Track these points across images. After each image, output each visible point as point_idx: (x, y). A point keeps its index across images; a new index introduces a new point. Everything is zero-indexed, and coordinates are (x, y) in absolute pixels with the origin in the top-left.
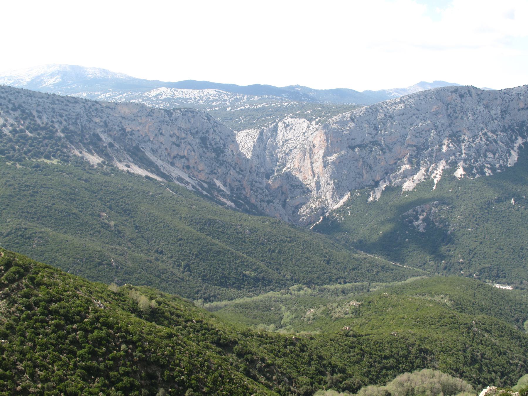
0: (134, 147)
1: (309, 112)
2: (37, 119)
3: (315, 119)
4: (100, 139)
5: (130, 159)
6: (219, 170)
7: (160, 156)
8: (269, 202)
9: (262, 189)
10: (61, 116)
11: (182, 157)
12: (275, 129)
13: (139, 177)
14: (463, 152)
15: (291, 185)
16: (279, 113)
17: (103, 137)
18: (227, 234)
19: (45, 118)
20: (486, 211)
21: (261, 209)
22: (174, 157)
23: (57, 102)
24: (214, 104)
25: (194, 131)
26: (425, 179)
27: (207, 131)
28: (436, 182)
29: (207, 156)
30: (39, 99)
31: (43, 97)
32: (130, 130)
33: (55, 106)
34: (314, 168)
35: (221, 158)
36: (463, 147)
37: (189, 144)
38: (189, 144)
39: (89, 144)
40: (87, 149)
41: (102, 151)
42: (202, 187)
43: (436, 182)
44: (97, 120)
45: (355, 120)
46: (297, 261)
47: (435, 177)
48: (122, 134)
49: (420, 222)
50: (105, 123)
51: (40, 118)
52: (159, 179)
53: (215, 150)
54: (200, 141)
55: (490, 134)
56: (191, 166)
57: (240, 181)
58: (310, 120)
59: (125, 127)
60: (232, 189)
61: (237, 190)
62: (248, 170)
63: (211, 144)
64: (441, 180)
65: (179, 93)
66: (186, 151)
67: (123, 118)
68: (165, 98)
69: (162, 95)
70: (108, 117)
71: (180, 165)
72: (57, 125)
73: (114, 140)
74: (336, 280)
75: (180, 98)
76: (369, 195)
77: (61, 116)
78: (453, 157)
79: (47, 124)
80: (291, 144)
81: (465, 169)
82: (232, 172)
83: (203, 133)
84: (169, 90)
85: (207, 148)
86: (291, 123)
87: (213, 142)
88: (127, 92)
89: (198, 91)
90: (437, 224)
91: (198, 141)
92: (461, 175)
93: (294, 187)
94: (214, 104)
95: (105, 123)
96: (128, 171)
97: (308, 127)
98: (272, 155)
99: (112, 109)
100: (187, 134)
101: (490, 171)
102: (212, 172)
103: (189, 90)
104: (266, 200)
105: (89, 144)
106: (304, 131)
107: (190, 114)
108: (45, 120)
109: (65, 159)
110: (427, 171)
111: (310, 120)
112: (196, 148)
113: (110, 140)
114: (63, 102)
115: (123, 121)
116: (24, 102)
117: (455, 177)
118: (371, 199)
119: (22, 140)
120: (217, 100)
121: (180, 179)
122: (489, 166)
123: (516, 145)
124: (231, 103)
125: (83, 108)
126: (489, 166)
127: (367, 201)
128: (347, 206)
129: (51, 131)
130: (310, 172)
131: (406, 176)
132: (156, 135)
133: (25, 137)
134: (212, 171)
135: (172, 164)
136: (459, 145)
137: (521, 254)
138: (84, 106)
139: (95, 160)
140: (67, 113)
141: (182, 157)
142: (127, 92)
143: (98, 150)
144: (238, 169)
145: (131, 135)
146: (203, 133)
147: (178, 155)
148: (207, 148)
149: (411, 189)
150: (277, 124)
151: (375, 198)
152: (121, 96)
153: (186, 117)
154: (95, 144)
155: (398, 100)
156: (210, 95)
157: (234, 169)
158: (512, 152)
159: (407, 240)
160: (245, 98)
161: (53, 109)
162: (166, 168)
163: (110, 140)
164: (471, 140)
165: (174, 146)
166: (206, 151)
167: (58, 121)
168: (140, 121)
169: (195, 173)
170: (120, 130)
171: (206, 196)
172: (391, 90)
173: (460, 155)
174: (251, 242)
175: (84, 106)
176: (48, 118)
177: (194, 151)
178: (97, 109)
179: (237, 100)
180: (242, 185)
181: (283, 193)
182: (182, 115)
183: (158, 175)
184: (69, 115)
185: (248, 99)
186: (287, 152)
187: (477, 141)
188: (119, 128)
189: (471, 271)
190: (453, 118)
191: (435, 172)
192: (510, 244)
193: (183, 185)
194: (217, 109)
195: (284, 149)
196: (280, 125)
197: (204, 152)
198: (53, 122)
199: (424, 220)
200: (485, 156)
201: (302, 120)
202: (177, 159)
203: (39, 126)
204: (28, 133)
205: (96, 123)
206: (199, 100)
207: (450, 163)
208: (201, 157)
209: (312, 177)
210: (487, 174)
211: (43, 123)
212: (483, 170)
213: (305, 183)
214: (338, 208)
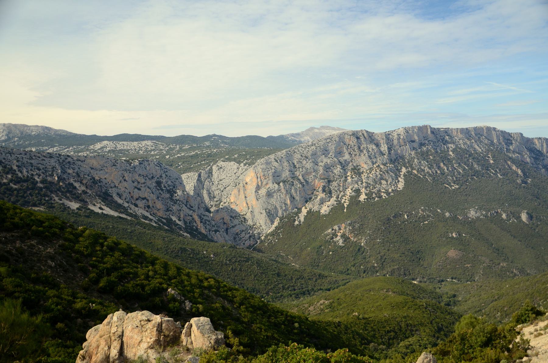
0: (104, 193)
1: (236, 156)
2: (17, 172)
3: (242, 162)
4: (75, 188)
5: (102, 203)
6: (174, 208)
7: (125, 199)
8: (216, 231)
9: (209, 221)
10: (39, 170)
11: (143, 199)
12: (210, 173)
13: (112, 217)
14: (364, 181)
15: (231, 217)
16: (212, 158)
17: (77, 185)
18: (197, 259)
19: (25, 171)
20: (388, 225)
21: (210, 237)
22: (137, 199)
23: (34, 158)
24: (152, 153)
25: (150, 177)
26: (337, 204)
27: (161, 176)
28: (346, 206)
29: (162, 196)
30: (18, 156)
31: (21, 154)
32: (99, 179)
33: (32, 161)
34: (248, 202)
35: (174, 198)
36: (363, 177)
37: (149, 187)
38: (149, 187)
39: (66, 192)
40: (65, 196)
41: (78, 197)
42: (162, 222)
43: (346, 206)
44: (70, 171)
45: (279, 161)
46: (255, 276)
47: (345, 202)
48: (93, 182)
49: (338, 238)
50: (77, 174)
51: (21, 172)
52: (129, 218)
53: (169, 191)
54: (156, 185)
55: (382, 166)
56: (151, 206)
57: (191, 216)
58: (239, 163)
59: (94, 176)
60: (185, 223)
61: (190, 223)
62: (197, 206)
63: (165, 187)
64: (349, 204)
65: (121, 145)
66: (146, 194)
67: (92, 168)
68: (109, 150)
69: (106, 147)
70: (79, 168)
71: (143, 206)
72: (36, 178)
73: (87, 187)
74: (288, 288)
75: (122, 150)
76: (295, 220)
77: (39, 170)
78: (357, 186)
79: (28, 176)
80: (225, 182)
81: (366, 194)
82: (184, 208)
83: (158, 178)
84: (111, 143)
85: (162, 190)
86: (223, 166)
87: (166, 185)
88: (72, 146)
89: (137, 143)
90: (352, 239)
91: (154, 184)
92: (364, 199)
93: (233, 218)
94: (152, 153)
95: (77, 174)
96: (102, 213)
97: (238, 168)
98: (210, 193)
99: (82, 161)
100: (146, 180)
101: (385, 195)
102: (168, 210)
103: (128, 143)
104: (213, 229)
105: (66, 192)
106: (235, 172)
107: (146, 163)
108: (25, 173)
109: (51, 206)
110: (338, 197)
111: (239, 163)
112: (154, 190)
113: (83, 188)
114: (39, 157)
115: (92, 171)
116: (4, 159)
117: (360, 201)
118: (297, 223)
119: (8, 192)
120: (154, 150)
121: (146, 218)
122: (384, 190)
123: (402, 173)
124: (167, 152)
125: (58, 162)
126: (384, 190)
127: (294, 225)
128: (279, 230)
129: (33, 183)
130: (245, 205)
131: (322, 202)
132: (120, 182)
133: (11, 190)
134: (167, 209)
135: (136, 205)
136: (360, 176)
137: (418, 256)
138: (58, 160)
139: (74, 205)
140: (44, 167)
141: (143, 199)
142: (72, 146)
143: (74, 196)
144: (188, 206)
145: (100, 182)
146: (158, 178)
147: (140, 197)
148: (162, 190)
149: (327, 213)
150: (211, 168)
151: (300, 222)
152: (68, 149)
153: (142, 165)
154: (70, 192)
155: (310, 143)
156: (148, 146)
157: (186, 206)
158: (399, 179)
159: (331, 253)
160: (178, 147)
161: (31, 163)
162: (133, 209)
163: (83, 188)
164: (368, 172)
165: (136, 190)
166: (162, 192)
167: (37, 174)
168: (106, 171)
169: (155, 211)
170: (91, 179)
171: (167, 230)
172: (288, 135)
173: (361, 184)
174: (216, 264)
175: (58, 160)
176: (28, 172)
177: (153, 193)
178: (69, 162)
179: (172, 149)
180: (193, 219)
181: (224, 223)
182: (140, 164)
183: (127, 215)
184: (46, 168)
185: (180, 148)
186: (222, 189)
187: (373, 172)
188: (89, 178)
189: (385, 272)
190: (353, 156)
191: (344, 198)
192: (409, 250)
193: (148, 222)
194: (158, 157)
195: (220, 187)
196: (214, 168)
197: (160, 193)
198: (32, 175)
199: (342, 236)
200: (381, 183)
201: (232, 163)
202: (139, 200)
203: (21, 178)
204: (12, 185)
205: (69, 174)
206: (139, 151)
207: (355, 190)
208: (158, 198)
209: (247, 208)
210: (384, 197)
211: (24, 176)
212: (380, 194)
213: (241, 214)
214: (271, 232)
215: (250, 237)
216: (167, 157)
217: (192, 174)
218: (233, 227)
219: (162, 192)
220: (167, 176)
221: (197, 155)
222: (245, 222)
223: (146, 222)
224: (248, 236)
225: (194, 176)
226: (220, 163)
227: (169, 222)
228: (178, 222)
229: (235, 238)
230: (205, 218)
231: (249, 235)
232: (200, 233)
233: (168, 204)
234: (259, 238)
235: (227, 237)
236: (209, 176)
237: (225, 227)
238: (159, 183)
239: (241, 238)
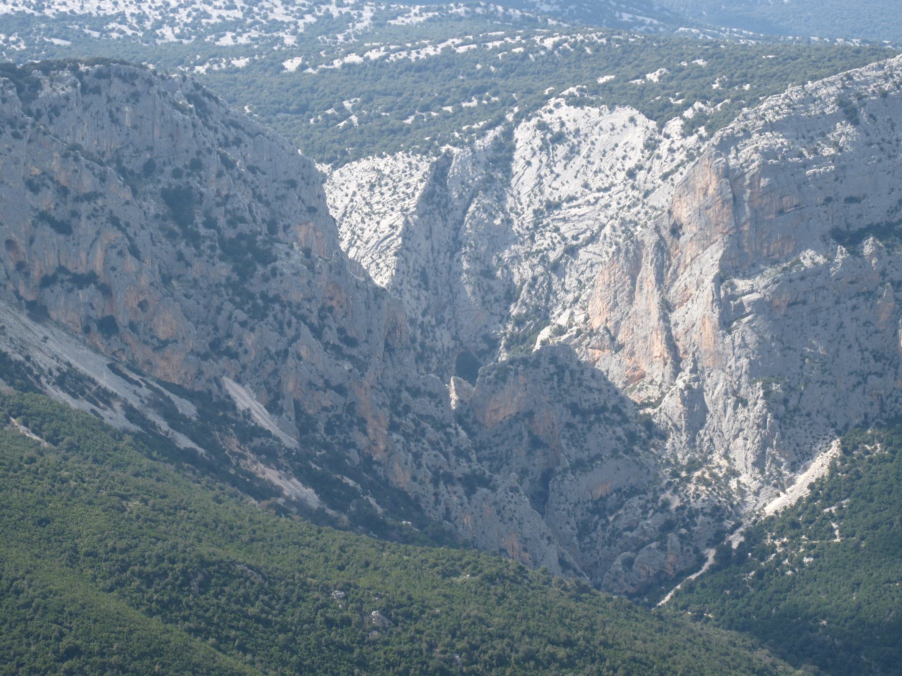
1: (653, 77)
3: (679, 111)
6: (250, 339)
8: (472, 483)
9: (441, 426)
12: (502, 155)
15: (574, 409)
18: (284, 629)
21: (436, 515)
22: (47, 282)
24: (227, 40)
25: (135, 165)
27: (196, 165)
29: (194, 273)
34: (677, 331)
35: (255, 286)
37: (114, 221)
45: (863, 115)
53: (230, 250)
54: (163, 209)
56: (122, 319)
57: (341, 390)
60: (305, 426)
61: (329, 430)
63: (210, 223)
66: (99, 253)
75: (72, 17)
80: (576, 221)
82: (307, 346)
83: (177, 174)
85: (194, 239)
86: (571, 126)
91: (153, 206)
93: (584, 414)
94: (227, 40)
97: (651, 145)
98: (488, 273)
102: (216, 349)
104: (458, 473)
106: (630, 164)
107: (117, 88)
111: (660, 114)
112: (142, 239)
124: (301, 38)
128: (828, 500)
130: (659, 348)
144: (331, 336)
146: (177, 174)
147: (62, 269)
148: (194, 239)
150: (509, 134)
157: (317, 333)
165: (47, 231)
166: (189, 252)
169: (141, 353)
171: (189, 455)
177: (135, 253)
181: (536, 443)
185: (379, 21)
193: (86, 406)
195: (542, 242)
196: (525, 136)
197: (180, 257)
201: (624, 114)
202: (57, 288)
206: (159, 25)
208: (166, 280)
213: (634, 397)
214: (787, 511)
215: (669, 526)
216: (292, 65)
217: (401, 160)
218: (579, 466)
219: (189, 252)
220: (229, 164)
221: (448, 60)
222: (645, 445)
223: (73, 404)
224: (652, 522)
225: (408, 171)
226: (562, 114)
227: (216, 410)
229: (584, 530)
231: (660, 518)
232: (381, 488)
233: (221, 319)
234: (718, 538)
235: (535, 524)
236: (490, 179)
237: (539, 461)
238: (179, 202)
239: (616, 534)
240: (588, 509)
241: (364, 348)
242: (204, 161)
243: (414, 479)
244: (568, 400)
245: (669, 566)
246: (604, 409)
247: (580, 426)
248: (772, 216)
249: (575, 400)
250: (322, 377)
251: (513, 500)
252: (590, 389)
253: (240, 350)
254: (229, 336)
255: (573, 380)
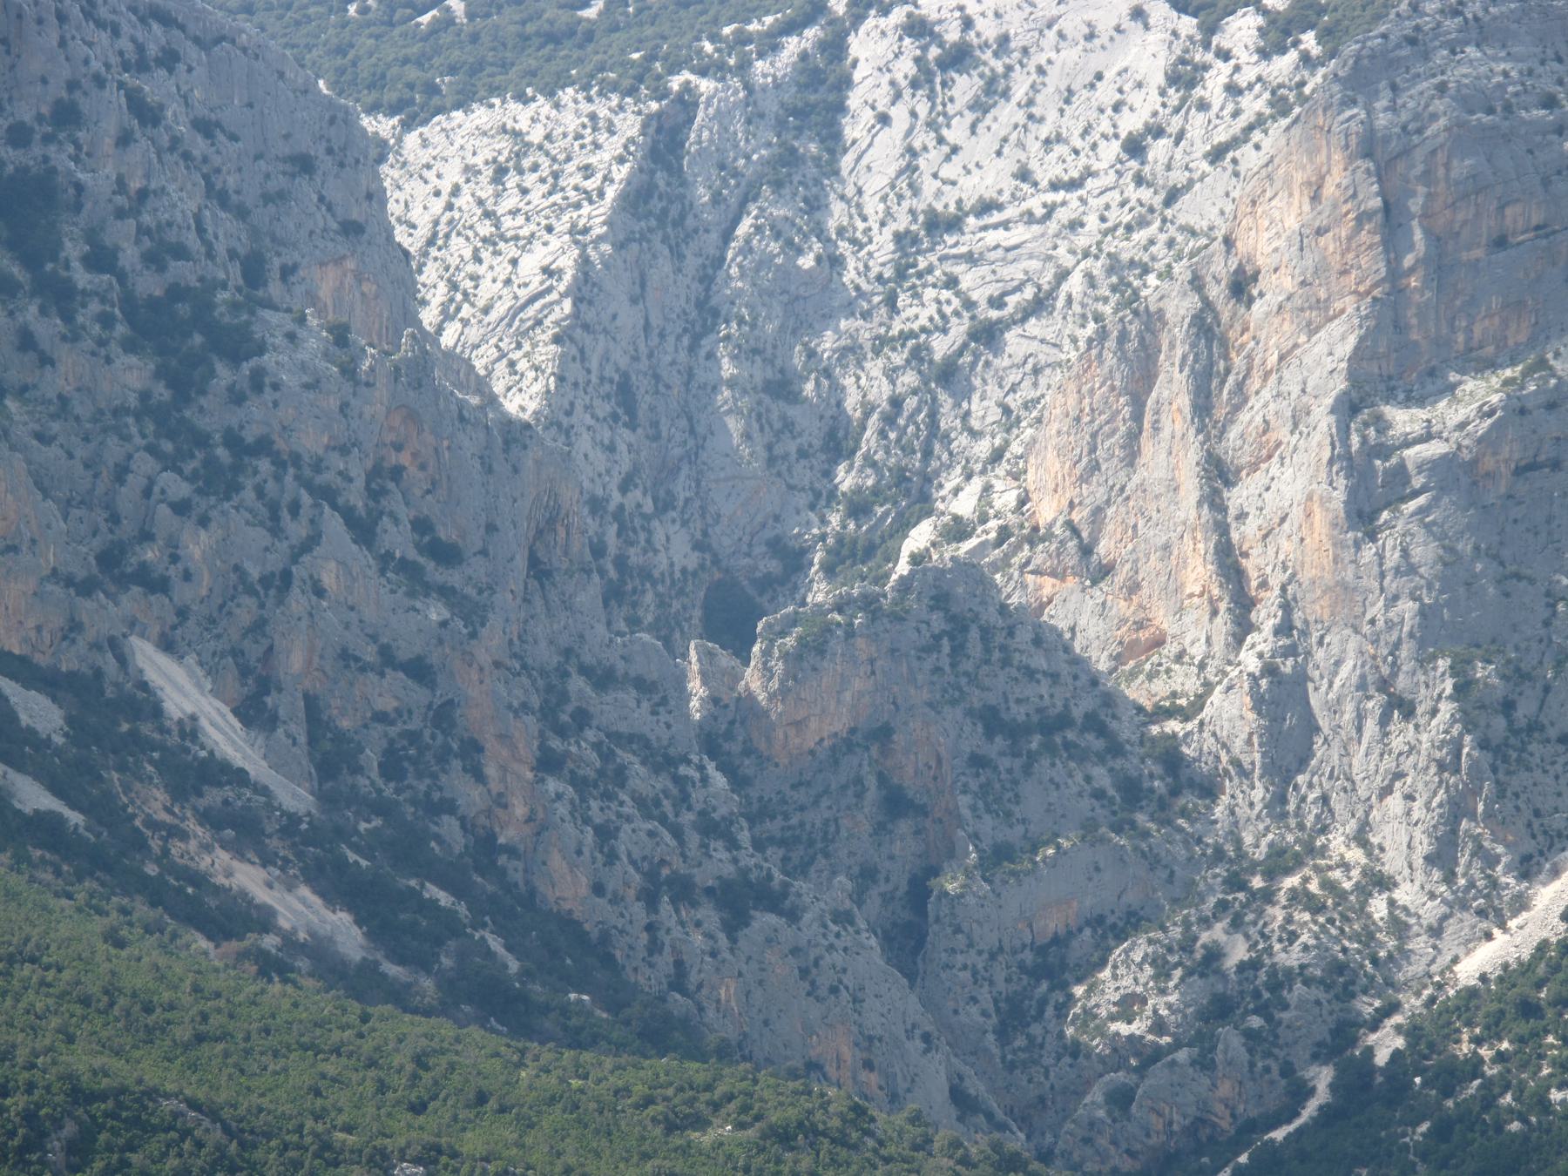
6: (197, 545)
8: (739, 901)
9: (664, 761)
15: (991, 720)
21: (650, 978)
29: (55, 382)
34: (1245, 533)
35: (211, 414)
57: (419, 671)
60: (330, 759)
61: (392, 767)
63: (101, 259)
82: (337, 563)
85: (61, 297)
93: (1016, 733)
97: (1184, 76)
98: (783, 388)
104: (705, 876)
106: (1131, 123)
130: (1199, 572)
134: (109, 559)
144: (397, 539)
148: (61, 297)
150: (835, 47)
157: (363, 530)
166: (47, 329)
195: (916, 313)
197: (26, 341)
209: (1222, 626)
214: (1510, 975)
219: (47, 329)
225: (587, 139)
228: (226, 737)
230: (621, 710)
234: (1342, 1039)
236: (790, 158)
240: (1022, 967)
241: (478, 568)
242: (84, 105)
243: (598, 889)
244: (976, 699)
245: (1219, 1108)
246: (1064, 721)
247: (1005, 763)
248: (1478, 253)
249: (992, 699)
250: (374, 638)
251: (839, 944)
252: (1030, 673)
253: (173, 572)
254: (146, 536)
255: (988, 650)
